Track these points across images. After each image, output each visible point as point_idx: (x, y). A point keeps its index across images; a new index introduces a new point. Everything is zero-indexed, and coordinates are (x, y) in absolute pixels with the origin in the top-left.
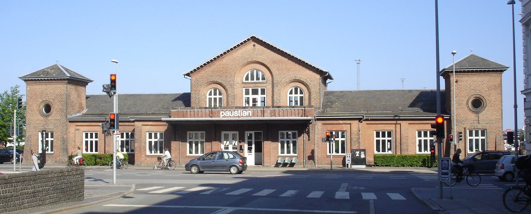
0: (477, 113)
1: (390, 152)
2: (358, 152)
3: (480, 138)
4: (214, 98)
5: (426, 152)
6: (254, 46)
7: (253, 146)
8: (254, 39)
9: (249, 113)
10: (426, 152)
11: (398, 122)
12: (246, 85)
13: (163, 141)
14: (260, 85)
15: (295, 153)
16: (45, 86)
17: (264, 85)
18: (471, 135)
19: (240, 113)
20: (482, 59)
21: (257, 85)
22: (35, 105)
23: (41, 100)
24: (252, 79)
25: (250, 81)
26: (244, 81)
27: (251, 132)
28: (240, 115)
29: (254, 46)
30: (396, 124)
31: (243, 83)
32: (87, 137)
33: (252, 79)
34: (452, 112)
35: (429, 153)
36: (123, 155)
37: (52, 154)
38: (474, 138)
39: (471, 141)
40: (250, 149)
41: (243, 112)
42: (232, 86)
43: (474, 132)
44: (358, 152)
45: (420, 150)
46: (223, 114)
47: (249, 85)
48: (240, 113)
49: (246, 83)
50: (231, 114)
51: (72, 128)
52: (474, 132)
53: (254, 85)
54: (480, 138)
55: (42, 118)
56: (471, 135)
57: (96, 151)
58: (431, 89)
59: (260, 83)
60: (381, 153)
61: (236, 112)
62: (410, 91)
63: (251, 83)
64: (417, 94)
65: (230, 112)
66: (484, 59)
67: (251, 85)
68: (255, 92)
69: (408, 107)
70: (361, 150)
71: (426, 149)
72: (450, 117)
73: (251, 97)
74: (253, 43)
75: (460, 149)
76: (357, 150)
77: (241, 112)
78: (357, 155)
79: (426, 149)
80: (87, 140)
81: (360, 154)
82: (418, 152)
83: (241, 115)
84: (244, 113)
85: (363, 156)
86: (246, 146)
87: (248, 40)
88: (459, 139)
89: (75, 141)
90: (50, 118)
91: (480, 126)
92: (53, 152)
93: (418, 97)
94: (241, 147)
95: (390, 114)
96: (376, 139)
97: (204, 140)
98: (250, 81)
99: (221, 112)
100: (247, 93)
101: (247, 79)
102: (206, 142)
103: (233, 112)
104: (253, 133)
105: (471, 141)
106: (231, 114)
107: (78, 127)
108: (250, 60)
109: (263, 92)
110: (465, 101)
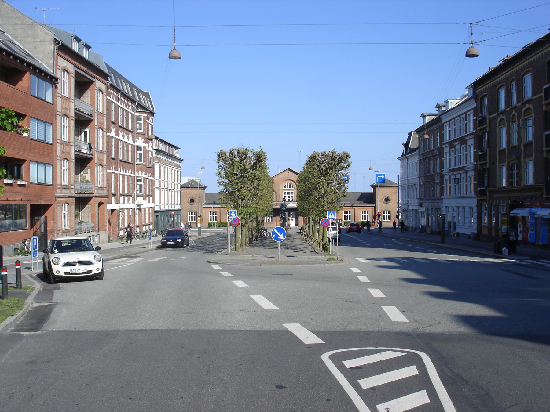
0: (387, 204)
1: (350, 221)
2: (339, 221)
3: (388, 214)
5: (365, 220)
6: (289, 172)
7: (294, 218)
8: (289, 169)
10: (365, 220)
11: (353, 207)
12: (285, 190)
14: (291, 190)
15: (389, 220)
16: (191, 190)
17: (293, 190)
18: (384, 213)
20: (389, 180)
21: (290, 190)
22: (186, 199)
23: (189, 197)
24: (287, 187)
25: (286, 188)
26: (284, 188)
27: (293, 212)
29: (289, 172)
30: (352, 208)
31: (283, 189)
32: (190, 214)
33: (287, 187)
34: (376, 203)
35: (367, 221)
38: (385, 214)
39: (384, 215)
40: (292, 219)
42: (278, 191)
43: (385, 212)
44: (339, 221)
45: (363, 220)
47: (286, 190)
49: (285, 189)
51: (204, 210)
52: (385, 212)
53: (289, 190)
54: (388, 214)
55: (189, 205)
56: (384, 213)
57: (216, 220)
58: (366, 192)
59: (291, 189)
60: (346, 221)
62: (357, 193)
63: (287, 189)
64: (360, 194)
66: (390, 181)
67: (287, 190)
68: (289, 193)
69: (357, 200)
70: (340, 220)
71: (365, 219)
72: (376, 205)
73: (287, 195)
74: (288, 171)
76: (338, 220)
78: (338, 222)
79: (365, 219)
80: (363, 215)
81: (340, 221)
82: (362, 221)
85: (341, 222)
86: (291, 219)
87: (286, 170)
88: (136, 226)
89: (205, 216)
90: (194, 205)
91: (388, 209)
92: (390, 220)
93: (361, 196)
94: (289, 218)
95: (349, 204)
96: (362, 215)
97: (272, 216)
98: (286, 188)
100: (285, 193)
101: (285, 187)
102: (273, 217)
104: (294, 212)
105: (384, 215)
107: (207, 210)
108: (287, 179)
109: (292, 193)
110: (382, 199)
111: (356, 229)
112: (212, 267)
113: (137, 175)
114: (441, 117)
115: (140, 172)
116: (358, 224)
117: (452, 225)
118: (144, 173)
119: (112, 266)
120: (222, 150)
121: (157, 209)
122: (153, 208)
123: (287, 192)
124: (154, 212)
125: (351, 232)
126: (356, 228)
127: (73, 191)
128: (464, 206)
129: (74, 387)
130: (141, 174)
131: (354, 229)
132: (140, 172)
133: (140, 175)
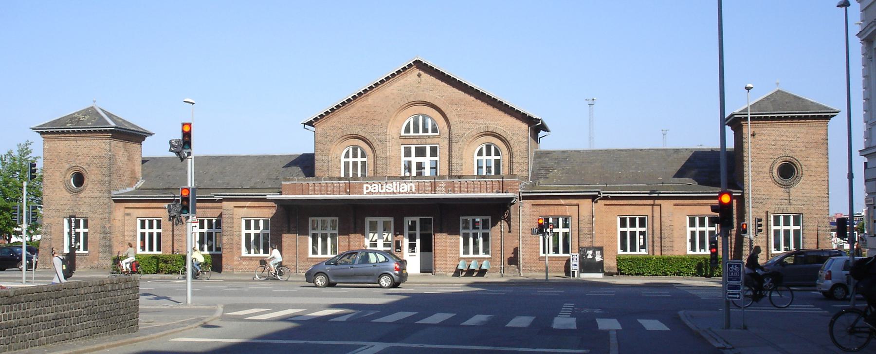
0: (787, 186)
1: (643, 252)
2: (590, 252)
3: (792, 228)
5: (703, 252)
6: (419, 75)
7: (418, 242)
8: (419, 64)
9: (411, 187)
10: (703, 252)
11: (657, 202)
12: (406, 141)
13: (268, 234)
14: (429, 141)
15: (487, 253)
16: (73, 142)
17: (436, 141)
18: (777, 223)
19: (396, 186)
20: (795, 97)
21: (424, 141)
22: (58, 174)
23: (67, 166)
24: (416, 130)
25: (412, 133)
26: (403, 134)
27: (414, 219)
28: (396, 190)
29: (419, 75)
30: (653, 205)
31: (401, 137)
32: (143, 227)
33: (416, 130)
34: (746, 185)
35: (708, 252)
36: (204, 256)
37: (86, 255)
38: (782, 228)
39: (777, 232)
40: (412, 246)
41: (401, 186)
42: (382, 142)
43: (782, 218)
44: (590, 252)
45: (693, 248)
46: (367, 188)
47: (410, 141)
48: (396, 186)
49: (405, 138)
50: (382, 189)
51: (119, 211)
52: (782, 218)
53: (419, 141)
54: (792, 228)
55: (69, 195)
56: (777, 223)
57: (159, 249)
58: (711, 147)
59: (429, 137)
60: (628, 252)
61: (389, 186)
62: (677, 151)
63: (415, 138)
64: (688, 155)
65: (380, 185)
66: (799, 98)
67: (415, 141)
68: (421, 152)
69: (674, 177)
70: (595, 249)
71: (702, 246)
72: (743, 193)
73: (414, 160)
74: (418, 71)
76: (589, 248)
77: (398, 185)
78: (590, 257)
79: (702, 246)
81: (594, 255)
82: (689, 252)
83: (398, 191)
84: (403, 186)
85: (598, 258)
86: (406, 242)
87: (410, 66)
89: (123, 234)
90: (82, 195)
91: (791, 209)
92: (87, 252)
93: (689, 160)
94: (397, 243)
95: (644, 188)
96: (620, 229)
97: (336, 232)
98: (412, 133)
99: (365, 186)
100: (408, 153)
101: (407, 130)
102: (339, 235)
103: (384, 185)
104: (417, 219)
105: (777, 232)
106: (382, 189)
107: (128, 211)
108: (412, 99)
109: (434, 152)
110: (768, 168)
112: (622, 326)
116: (823, 263)
125: (559, 316)
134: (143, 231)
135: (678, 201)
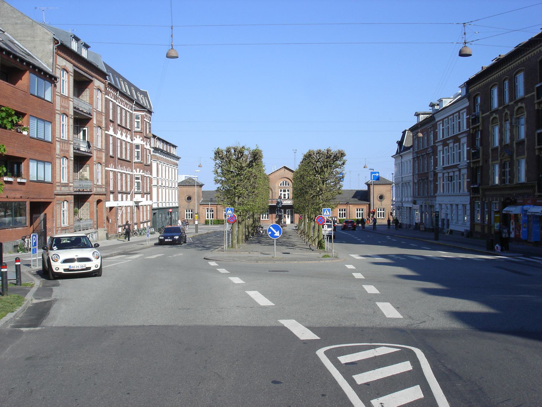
0: (381, 201)
1: (345, 218)
2: (334, 218)
3: (382, 212)
4: (340, 211)
5: (360, 218)
6: (285, 170)
7: (290, 216)
8: (285, 167)
10: (360, 218)
11: (348, 205)
12: (281, 188)
14: (287, 188)
15: (384, 217)
16: (188, 188)
17: (289, 188)
18: (378, 211)
20: (383, 178)
21: (286, 188)
22: (183, 197)
23: (186, 195)
24: (283, 185)
25: (282, 186)
26: (280, 186)
27: (288, 210)
29: (285, 170)
30: (347, 206)
31: (279, 187)
32: (187, 212)
33: (283, 185)
34: (371, 201)
35: (361, 218)
38: (380, 212)
39: (378, 213)
40: (288, 217)
42: (274, 188)
43: (380, 209)
44: (334, 218)
45: (357, 217)
47: (282, 188)
49: (281, 187)
51: (201, 207)
52: (380, 209)
53: (284, 188)
54: (382, 212)
55: (187, 203)
56: (378, 211)
57: (213, 218)
58: (361, 189)
59: (287, 187)
60: (341, 218)
62: (352, 190)
63: (283, 187)
64: (355, 192)
66: (384, 179)
67: (283, 188)
68: (285, 191)
69: (352, 198)
70: (335, 217)
71: (360, 217)
72: (370, 203)
73: (283, 193)
74: (284, 169)
75: (324, 352)
76: (333, 217)
78: (334, 219)
79: (360, 217)
81: (335, 219)
82: (357, 218)
85: (336, 220)
86: (287, 216)
87: (282, 168)
89: (202, 214)
90: (191, 203)
91: (382, 207)
92: (384, 218)
93: (355, 193)
94: (285, 216)
95: (344, 201)
96: (356, 212)
97: (268, 213)
98: (282, 186)
100: (281, 191)
101: (281, 185)
102: (269, 214)
104: (290, 210)
105: (378, 213)
107: (204, 207)
108: (283, 177)
109: (288, 190)
110: (376, 197)
111: (351, 226)
113: (135, 173)
114: (435, 116)
115: (138, 170)
116: (353, 221)
117: (445, 222)
118: (142, 171)
119: (111, 263)
120: (219, 148)
121: (155, 206)
122: (151, 206)
123: (282, 190)
124: (152, 209)
126: (351, 225)
127: (71, 189)
128: (457, 204)
129: (73, 382)
130: (139, 172)
131: (348, 226)
132: (138, 170)
133: (138, 173)
134: (357, 212)
135: (36, 201)
